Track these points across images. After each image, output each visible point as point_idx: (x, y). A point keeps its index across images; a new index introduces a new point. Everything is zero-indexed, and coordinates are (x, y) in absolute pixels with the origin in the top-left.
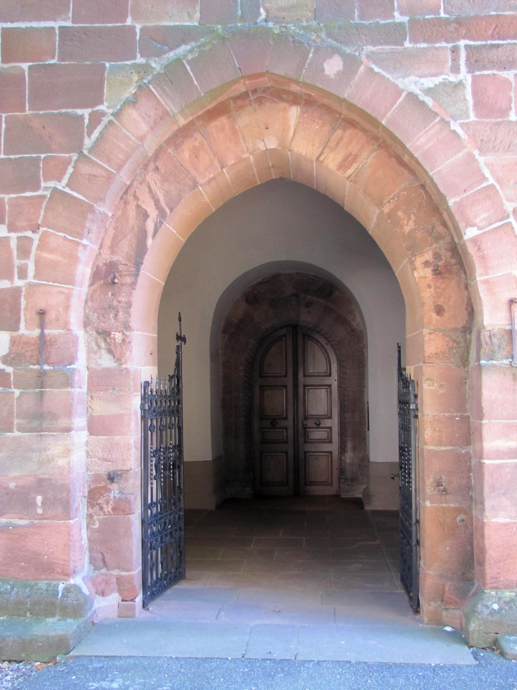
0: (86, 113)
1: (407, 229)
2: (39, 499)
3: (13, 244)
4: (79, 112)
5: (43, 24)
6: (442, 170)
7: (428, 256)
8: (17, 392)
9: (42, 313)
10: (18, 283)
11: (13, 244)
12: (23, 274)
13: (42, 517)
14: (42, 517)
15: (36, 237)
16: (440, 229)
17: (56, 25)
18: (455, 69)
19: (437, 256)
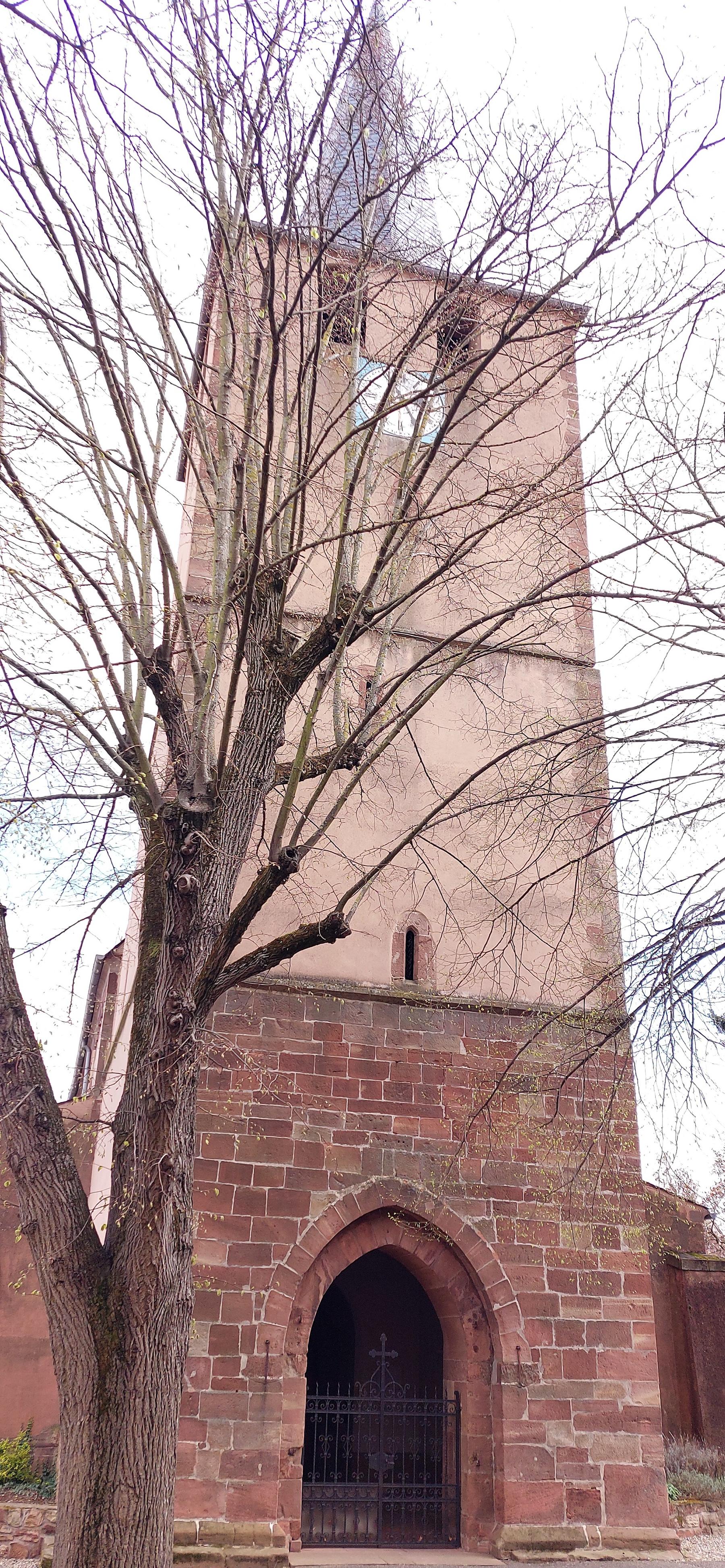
0: (299, 1219)
1: (460, 1298)
2: (260, 1466)
3: (253, 1298)
4: (295, 1219)
5: (277, 1165)
6: (482, 1268)
7: (470, 1316)
8: (251, 1394)
9: (267, 1343)
10: (255, 1322)
11: (253, 1298)
12: (258, 1317)
13: (261, 1478)
14: (261, 1478)
15: (267, 1294)
16: (476, 1299)
17: (285, 1166)
18: (488, 1214)
19: (475, 1315)
